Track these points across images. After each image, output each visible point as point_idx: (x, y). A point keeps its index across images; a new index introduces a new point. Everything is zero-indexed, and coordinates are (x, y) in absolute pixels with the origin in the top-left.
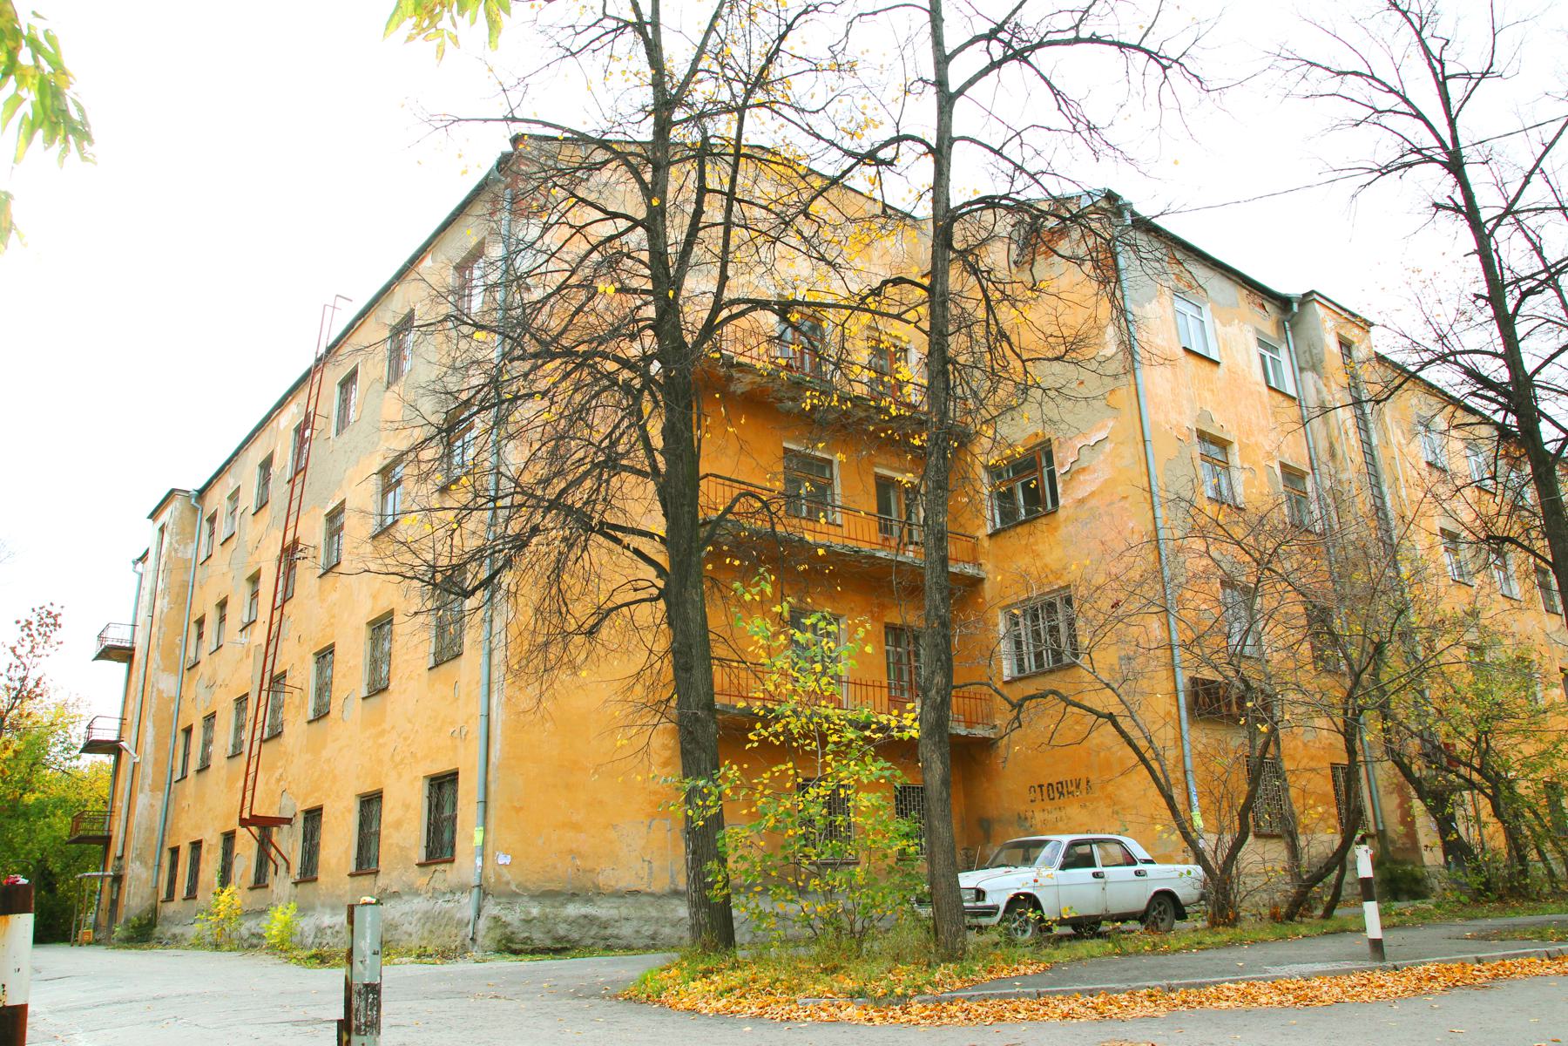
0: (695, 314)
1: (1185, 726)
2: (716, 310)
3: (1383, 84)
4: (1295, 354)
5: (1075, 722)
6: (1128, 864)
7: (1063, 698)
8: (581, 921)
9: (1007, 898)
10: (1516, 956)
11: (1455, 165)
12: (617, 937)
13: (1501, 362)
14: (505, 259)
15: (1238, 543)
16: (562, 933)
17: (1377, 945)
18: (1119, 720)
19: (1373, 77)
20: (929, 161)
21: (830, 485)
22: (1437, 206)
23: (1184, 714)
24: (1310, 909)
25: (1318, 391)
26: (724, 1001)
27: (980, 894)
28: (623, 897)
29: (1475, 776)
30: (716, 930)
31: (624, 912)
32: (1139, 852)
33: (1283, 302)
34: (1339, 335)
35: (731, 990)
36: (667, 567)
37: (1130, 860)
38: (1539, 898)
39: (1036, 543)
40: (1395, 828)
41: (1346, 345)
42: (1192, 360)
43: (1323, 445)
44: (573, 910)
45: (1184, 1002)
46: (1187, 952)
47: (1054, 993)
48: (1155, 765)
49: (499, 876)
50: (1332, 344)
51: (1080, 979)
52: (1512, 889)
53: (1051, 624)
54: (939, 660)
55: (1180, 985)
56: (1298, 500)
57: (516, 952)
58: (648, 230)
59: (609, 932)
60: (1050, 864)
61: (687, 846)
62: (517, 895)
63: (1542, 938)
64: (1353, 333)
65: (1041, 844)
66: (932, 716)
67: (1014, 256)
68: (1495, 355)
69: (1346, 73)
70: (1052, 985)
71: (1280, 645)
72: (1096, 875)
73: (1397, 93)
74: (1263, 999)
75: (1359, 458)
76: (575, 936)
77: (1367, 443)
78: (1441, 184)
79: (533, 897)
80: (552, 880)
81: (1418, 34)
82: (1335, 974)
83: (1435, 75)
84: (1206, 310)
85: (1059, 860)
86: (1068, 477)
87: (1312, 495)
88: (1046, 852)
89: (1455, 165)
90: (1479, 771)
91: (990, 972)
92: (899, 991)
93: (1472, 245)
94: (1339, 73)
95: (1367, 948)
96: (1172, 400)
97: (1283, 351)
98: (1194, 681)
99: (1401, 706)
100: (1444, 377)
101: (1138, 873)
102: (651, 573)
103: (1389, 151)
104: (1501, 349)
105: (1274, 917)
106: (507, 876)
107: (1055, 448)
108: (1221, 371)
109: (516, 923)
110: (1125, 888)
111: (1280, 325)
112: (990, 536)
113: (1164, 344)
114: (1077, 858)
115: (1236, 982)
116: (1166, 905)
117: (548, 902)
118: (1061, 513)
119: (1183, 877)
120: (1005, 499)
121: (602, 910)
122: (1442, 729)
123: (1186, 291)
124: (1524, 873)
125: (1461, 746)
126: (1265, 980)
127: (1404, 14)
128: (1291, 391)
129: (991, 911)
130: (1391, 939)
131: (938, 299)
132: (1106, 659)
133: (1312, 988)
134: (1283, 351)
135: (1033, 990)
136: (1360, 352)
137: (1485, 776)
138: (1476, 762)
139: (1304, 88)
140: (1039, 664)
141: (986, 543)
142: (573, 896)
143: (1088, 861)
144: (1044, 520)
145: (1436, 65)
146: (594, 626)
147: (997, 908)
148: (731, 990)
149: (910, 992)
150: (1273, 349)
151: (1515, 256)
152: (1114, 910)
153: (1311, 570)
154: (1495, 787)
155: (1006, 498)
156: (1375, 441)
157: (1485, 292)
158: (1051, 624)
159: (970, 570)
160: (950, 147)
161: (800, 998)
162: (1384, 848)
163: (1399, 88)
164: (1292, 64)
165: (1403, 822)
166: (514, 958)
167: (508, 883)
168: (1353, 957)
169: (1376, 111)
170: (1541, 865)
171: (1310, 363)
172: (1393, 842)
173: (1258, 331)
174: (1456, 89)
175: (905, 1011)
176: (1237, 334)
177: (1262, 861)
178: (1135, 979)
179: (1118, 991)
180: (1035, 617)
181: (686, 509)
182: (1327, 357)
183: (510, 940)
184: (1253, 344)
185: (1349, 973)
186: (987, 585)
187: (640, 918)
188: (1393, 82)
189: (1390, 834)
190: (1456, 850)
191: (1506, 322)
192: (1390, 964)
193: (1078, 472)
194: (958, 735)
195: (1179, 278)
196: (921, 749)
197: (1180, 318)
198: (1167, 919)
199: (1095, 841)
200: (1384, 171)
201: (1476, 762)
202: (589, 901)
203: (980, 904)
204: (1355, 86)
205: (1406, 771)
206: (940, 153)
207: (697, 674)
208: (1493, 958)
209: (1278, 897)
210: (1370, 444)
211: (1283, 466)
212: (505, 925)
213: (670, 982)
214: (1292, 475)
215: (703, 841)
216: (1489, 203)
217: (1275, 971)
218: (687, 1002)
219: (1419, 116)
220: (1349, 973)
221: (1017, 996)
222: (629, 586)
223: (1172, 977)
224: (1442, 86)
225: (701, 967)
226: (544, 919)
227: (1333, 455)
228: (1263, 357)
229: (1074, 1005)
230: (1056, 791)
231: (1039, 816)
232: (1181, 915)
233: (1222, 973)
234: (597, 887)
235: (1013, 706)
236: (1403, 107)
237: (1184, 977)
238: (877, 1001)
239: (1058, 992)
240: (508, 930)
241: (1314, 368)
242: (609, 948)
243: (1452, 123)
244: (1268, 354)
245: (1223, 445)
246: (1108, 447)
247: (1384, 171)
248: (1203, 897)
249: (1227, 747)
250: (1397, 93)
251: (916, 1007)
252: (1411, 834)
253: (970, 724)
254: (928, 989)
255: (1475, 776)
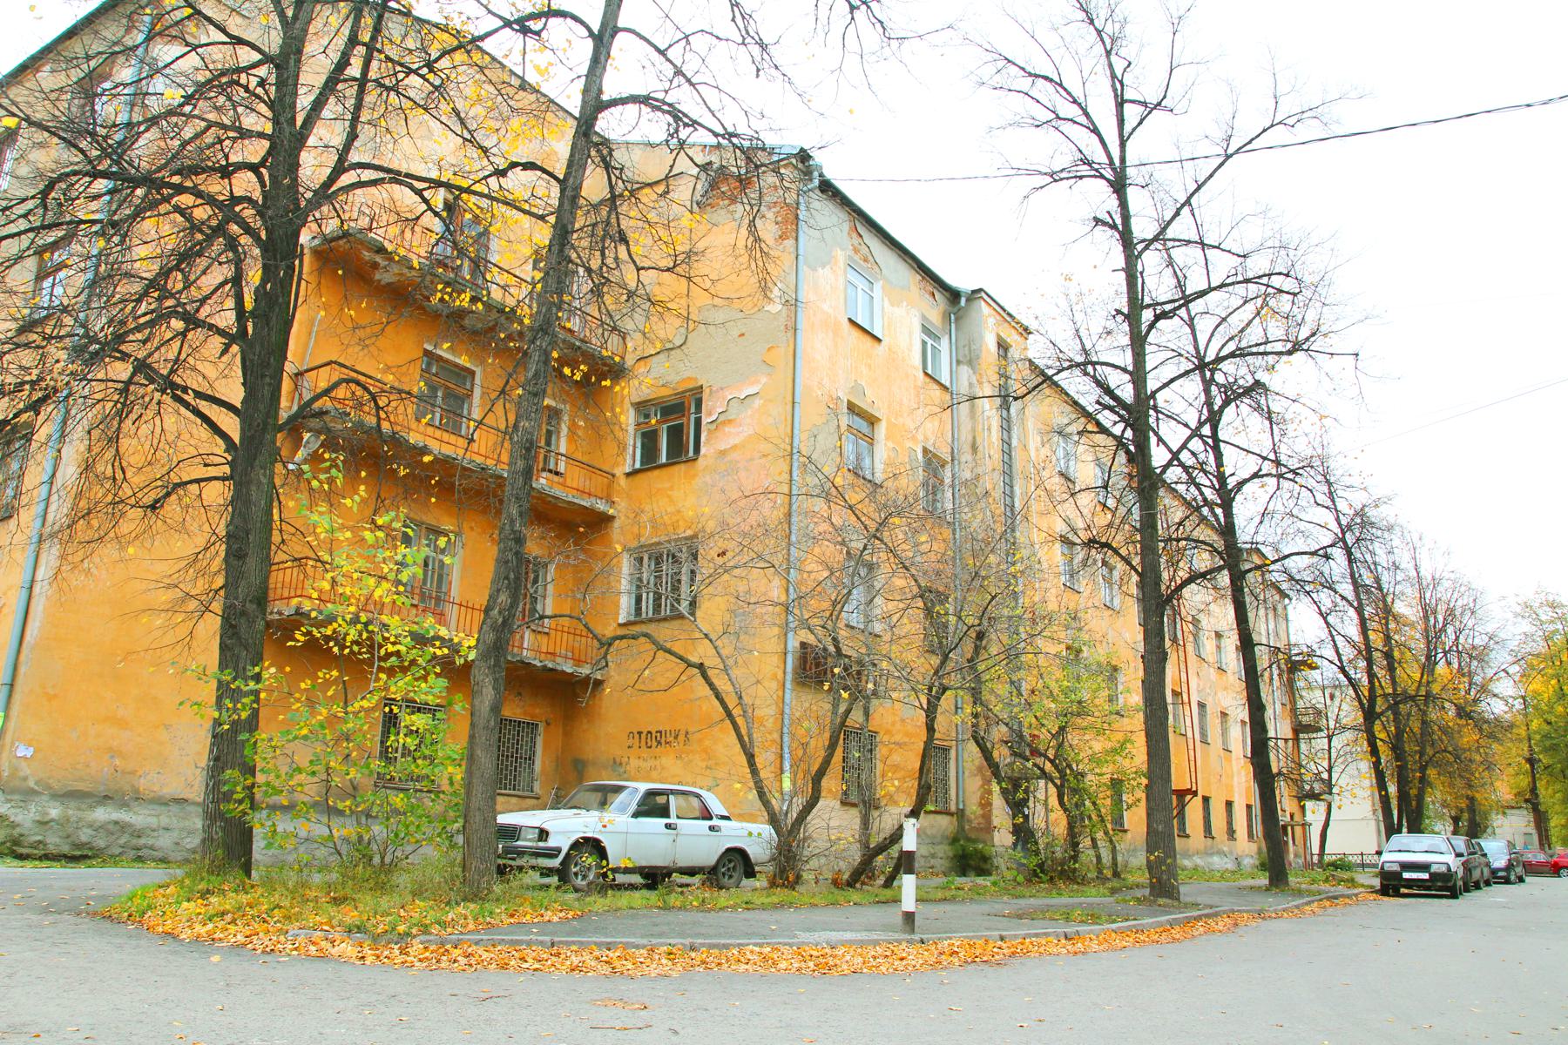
0: (313, 167)
1: (788, 685)
2: (340, 168)
3: (1069, 94)
4: (956, 347)
5: (667, 669)
6: (704, 818)
7: (654, 642)
8: (111, 827)
9: (570, 842)
10: (1037, 935)
11: (1119, 186)
12: (152, 848)
13: (1128, 377)
14: (1494, 872)
15: (851, 507)
16: (84, 839)
17: (909, 917)
18: (710, 673)
19: (1061, 85)
20: (589, 44)
21: (470, 396)
22: (1097, 221)
23: (789, 677)
24: (872, 877)
25: (971, 385)
26: (210, 926)
27: (543, 834)
28: (166, 804)
29: (1048, 767)
30: (230, 847)
31: (164, 821)
32: (717, 807)
33: (953, 295)
34: (999, 336)
35: (223, 913)
36: (236, 437)
37: (707, 815)
38: (1084, 881)
39: (672, 488)
40: (973, 809)
41: (1003, 346)
42: (856, 333)
43: (965, 436)
44: (102, 814)
45: (703, 962)
46: (738, 914)
47: (568, 944)
48: (740, 721)
49: (15, 770)
50: (991, 343)
51: (596, 931)
52: (1063, 872)
53: (672, 569)
54: (507, 578)
55: (703, 945)
56: (933, 487)
57: (21, 857)
58: (277, 67)
59: (142, 841)
60: (622, 810)
61: (211, 751)
62: (33, 792)
63: (1067, 919)
64: (1012, 337)
65: (618, 790)
66: (490, 637)
67: (698, 197)
68: (1124, 370)
69: (1037, 76)
70: (569, 935)
71: (889, 623)
72: (668, 826)
73: (1079, 105)
74: (783, 965)
75: (997, 456)
76: (101, 843)
77: (1007, 443)
78: (1099, 196)
79: (55, 796)
80: (81, 779)
81: (1108, 53)
82: (862, 944)
83: (1116, 96)
84: (878, 286)
85: (633, 807)
86: (713, 427)
87: (948, 481)
88: (622, 796)
89: (1119, 186)
90: (1052, 762)
91: (512, 916)
92: (401, 928)
93: (1120, 262)
94: (1030, 75)
95: (899, 919)
96: (830, 365)
97: (945, 341)
98: (803, 645)
99: (997, 691)
100: (1080, 387)
101: (712, 828)
102: (220, 446)
103: (1064, 159)
104: (1130, 368)
105: (836, 883)
106: (26, 770)
107: (705, 396)
108: (880, 349)
109: (28, 824)
110: (696, 842)
111: (946, 317)
112: (628, 475)
113: (830, 311)
114: (653, 806)
115: (761, 945)
116: (737, 861)
117: (73, 804)
118: (701, 462)
119: (756, 837)
120: (649, 440)
121: (138, 817)
122: (1028, 719)
123: (863, 266)
124: (1075, 858)
125: (1044, 735)
126: (791, 945)
127: (1099, 32)
128: (945, 380)
129: (553, 853)
130: (924, 913)
131: (569, 193)
132: (712, 612)
133: (835, 956)
134: (945, 341)
135: (547, 938)
136: (1014, 353)
137: (1056, 767)
138: (1051, 753)
139: (998, 80)
140: (657, 607)
141: (623, 481)
142: (106, 799)
143: (664, 812)
144: (682, 467)
145: (1118, 86)
146: (157, 501)
147: (559, 850)
148: (223, 913)
149: (414, 931)
150: (937, 338)
151: (1159, 286)
152: (682, 863)
153: (928, 548)
154: (1063, 776)
155: (649, 439)
156: (1014, 442)
157: (1126, 311)
158: (672, 569)
159: (601, 506)
160: (613, 37)
161: (293, 928)
162: (961, 828)
163: (1081, 100)
164: (990, 57)
165: (982, 805)
166: (16, 863)
167: (25, 779)
168: (886, 928)
169: (1058, 118)
170: (1091, 852)
171: (967, 358)
172: (969, 821)
173: (924, 317)
174: (1132, 113)
175: (403, 952)
176: (904, 315)
177: (834, 828)
178: (661, 935)
179: (637, 947)
180: (659, 561)
181: (267, 380)
182: (983, 355)
183: (16, 842)
184: (917, 329)
185: (876, 943)
186: (617, 524)
187: (182, 830)
188: (1077, 93)
189: (968, 812)
190: (1023, 834)
191: (1138, 342)
192: (917, 937)
193: (724, 423)
194: (563, 672)
195: (856, 251)
196: (474, 671)
197: (850, 289)
198: (735, 875)
199: (672, 792)
200: (1055, 177)
201: (1051, 753)
202: (124, 805)
203: (541, 844)
204: (1043, 90)
205: (987, 754)
206: (603, 39)
207: (252, 563)
208: (1016, 937)
209: (843, 865)
210: (1009, 445)
211: (925, 451)
212: (14, 825)
213: (161, 900)
214: (933, 463)
215: (230, 749)
216: (1143, 228)
217: (804, 937)
218: (169, 926)
219: (1095, 131)
220: (876, 943)
221: (529, 943)
222: (199, 459)
223: (698, 935)
224: (1120, 103)
225: (202, 886)
226: (63, 822)
227: (974, 448)
228: (924, 343)
229: (586, 957)
230: (655, 739)
231: (634, 763)
232: (750, 872)
233: (748, 935)
234: (137, 791)
235: (602, 644)
236: (1083, 120)
237: (711, 937)
238: (376, 938)
239: (574, 943)
240: (16, 832)
241: (970, 363)
242: (140, 859)
243: (1123, 145)
244: (930, 342)
245: (872, 421)
246: (757, 402)
247: (1055, 177)
248: (773, 859)
249: (812, 712)
250: (1079, 105)
251: (416, 946)
252: (987, 817)
253: (578, 662)
254: (435, 929)
255: (1048, 767)
